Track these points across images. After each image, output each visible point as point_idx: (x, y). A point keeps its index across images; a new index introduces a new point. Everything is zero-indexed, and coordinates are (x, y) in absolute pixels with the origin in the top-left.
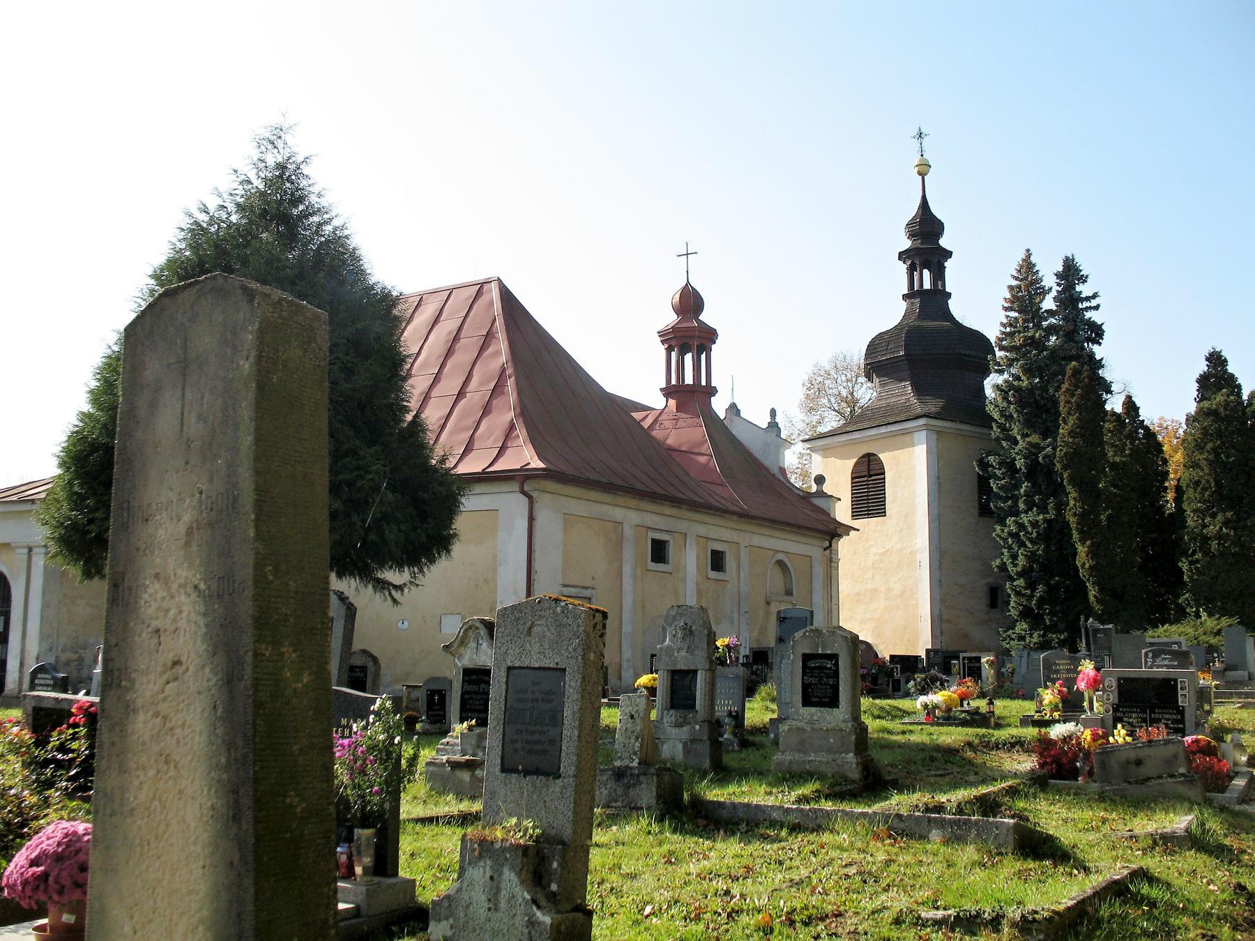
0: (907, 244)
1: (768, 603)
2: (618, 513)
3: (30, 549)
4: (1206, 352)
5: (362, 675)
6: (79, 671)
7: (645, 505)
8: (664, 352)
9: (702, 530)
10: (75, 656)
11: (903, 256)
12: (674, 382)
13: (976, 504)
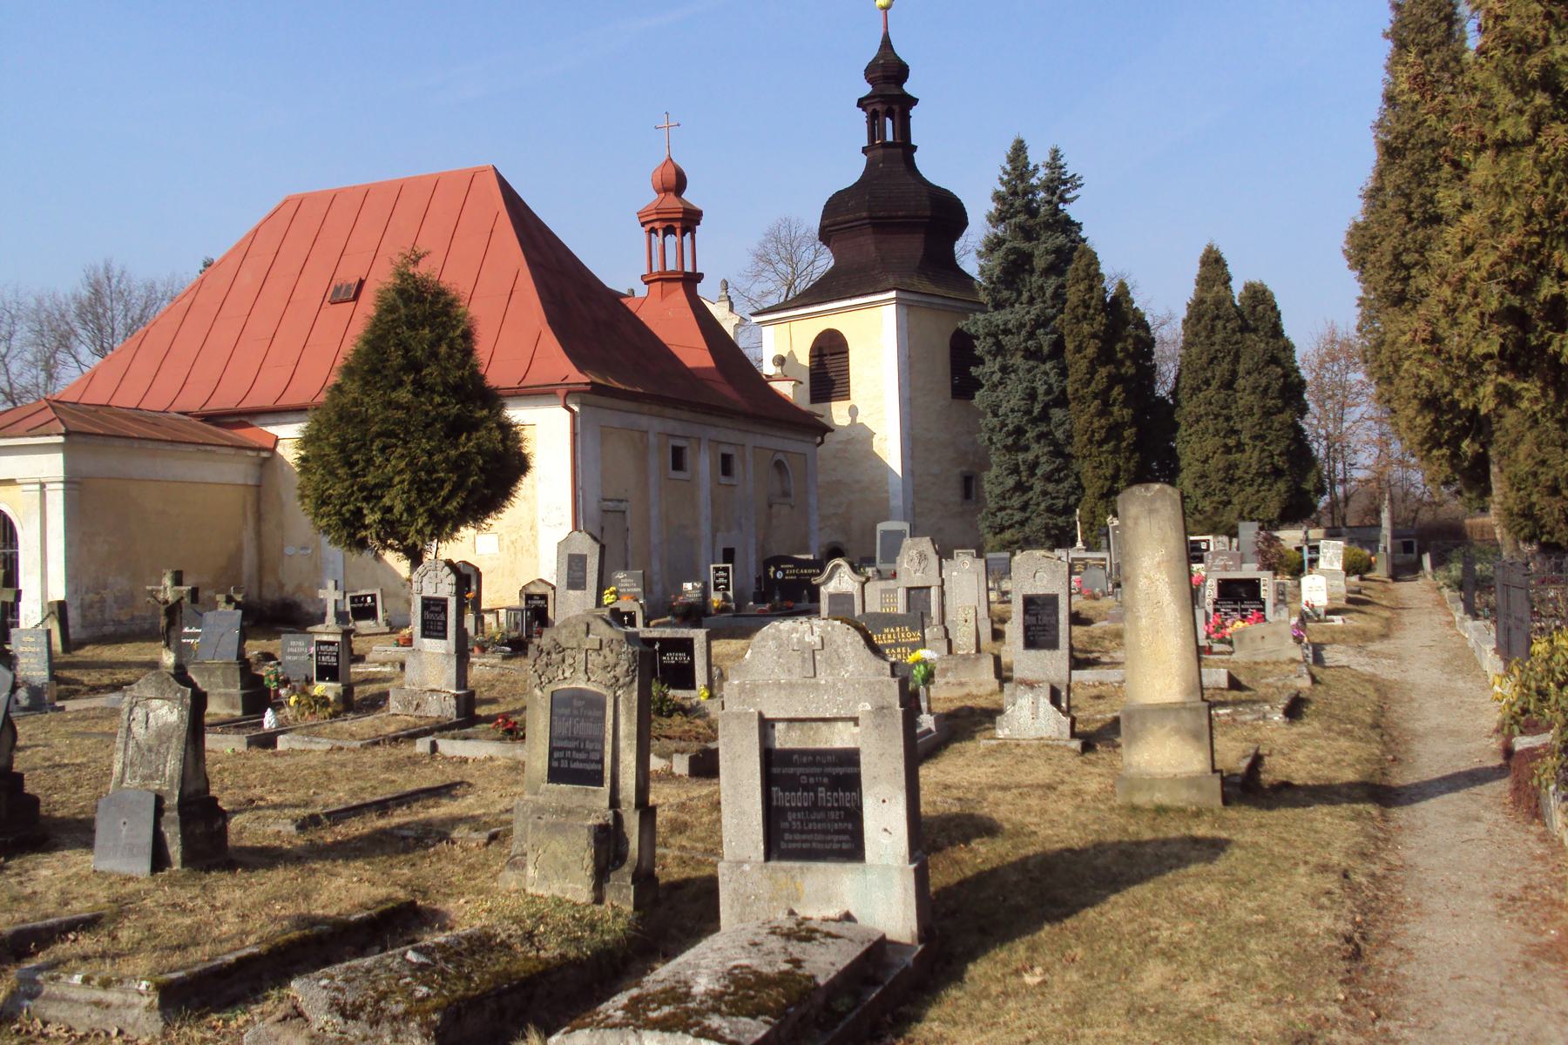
0: (866, 89)
1: (770, 506)
2: (644, 422)
3: (43, 485)
4: (1201, 252)
5: (543, 602)
6: (102, 611)
7: (669, 412)
8: (645, 237)
9: (713, 433)
10: (97, 598)
11: (861, 103)
12: (655, 270)
13: (949, 384)
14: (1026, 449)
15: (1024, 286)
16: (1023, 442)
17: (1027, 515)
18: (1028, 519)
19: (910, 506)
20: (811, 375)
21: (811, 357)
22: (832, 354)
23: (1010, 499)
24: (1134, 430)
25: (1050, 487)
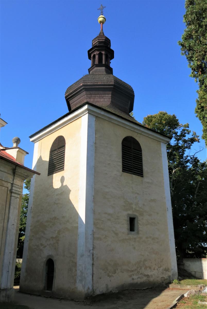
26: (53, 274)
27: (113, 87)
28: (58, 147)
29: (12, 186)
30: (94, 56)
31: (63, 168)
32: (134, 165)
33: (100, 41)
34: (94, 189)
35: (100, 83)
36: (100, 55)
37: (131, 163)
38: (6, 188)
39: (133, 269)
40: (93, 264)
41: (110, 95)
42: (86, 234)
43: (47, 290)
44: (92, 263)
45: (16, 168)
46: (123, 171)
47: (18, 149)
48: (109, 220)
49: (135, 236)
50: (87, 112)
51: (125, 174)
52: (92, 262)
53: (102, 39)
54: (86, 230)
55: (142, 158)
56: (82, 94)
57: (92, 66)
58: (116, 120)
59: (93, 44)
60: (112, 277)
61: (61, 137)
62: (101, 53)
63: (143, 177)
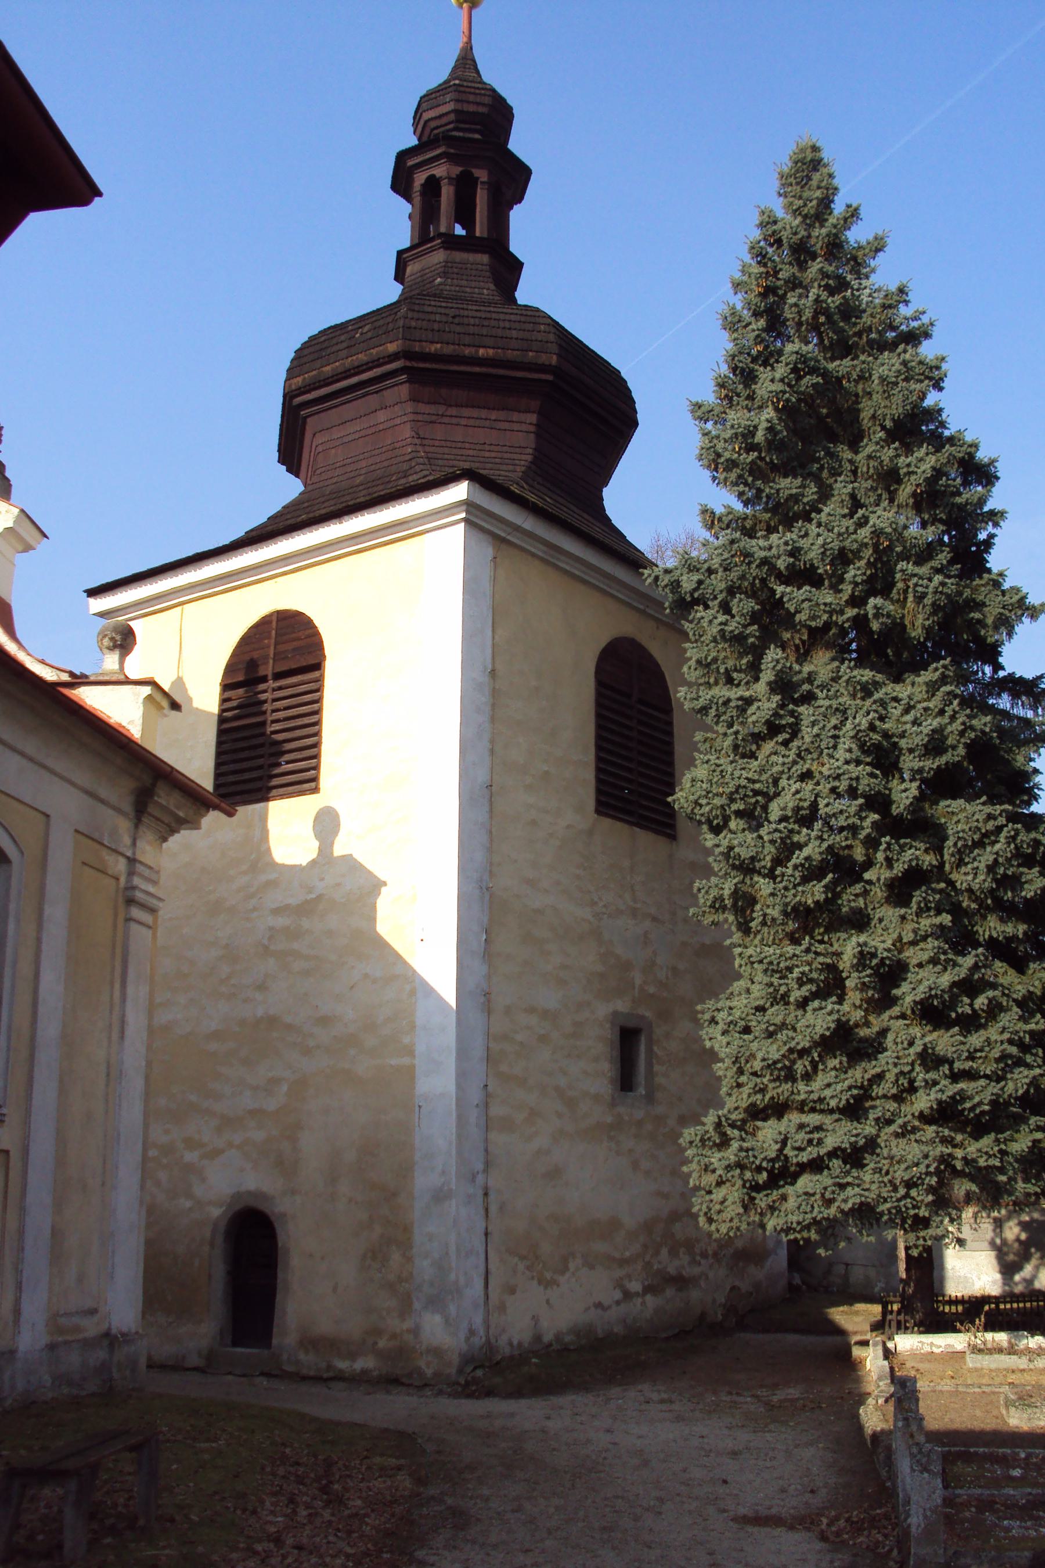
14: (860, 921)
15: (835, 473)
16: (850, 899)
17: (869, 1129)
18: (872, 1144)
19: (475, 1095)
20: (221, 733)
21: (226, 687)
22: (278, 676)
23: (808, 1077)
24: (970, 1012)
25: (944, 1041)
26: (274, 1276)
27: (550, 378)
28: (278, 669)
29: (131, 873)
30: (432, 186)
31: (315, 779)
32: (641, 780)
33: (467, 108)
34: (487, 897)
35: (491, 352)
36: (465, 186)
37: (630, 770)
38: (113, 882)
39: (627, 1254)
40: (486, 1234)
41: (533, 418)
42: (459, 1101)
43: (235, 1344)
44: (483, 1230)
45: (154, 785)
46: (598, 812)
47: (147, 690)
48: (543, 1039)
49: (639, 1114)
50: (463, 515)
51: (607, 822)
52: (484, 1225)
53: (478, 99)
54: (459, 1086)
55: (670, 744)
56: (390, 396)
57: (416, 241)
58: (578, 559)
59: (427, 116)
60: (555, 1287)
61: (285, 619)
62: (471, 174)
63: (673, 837)
